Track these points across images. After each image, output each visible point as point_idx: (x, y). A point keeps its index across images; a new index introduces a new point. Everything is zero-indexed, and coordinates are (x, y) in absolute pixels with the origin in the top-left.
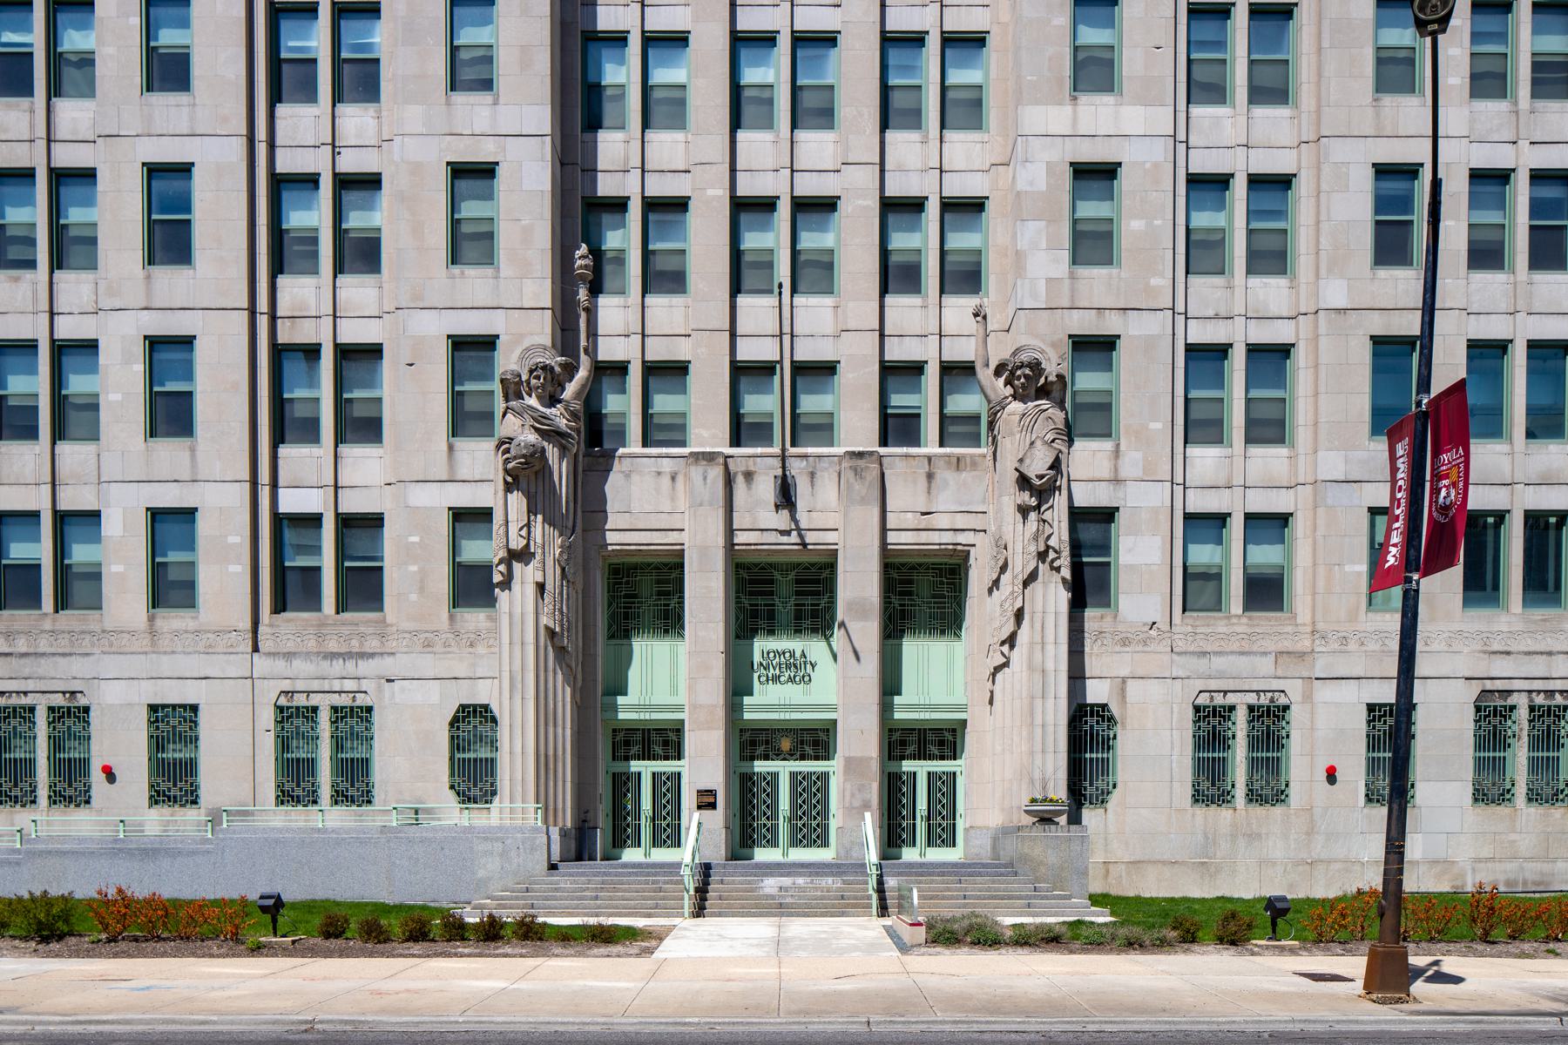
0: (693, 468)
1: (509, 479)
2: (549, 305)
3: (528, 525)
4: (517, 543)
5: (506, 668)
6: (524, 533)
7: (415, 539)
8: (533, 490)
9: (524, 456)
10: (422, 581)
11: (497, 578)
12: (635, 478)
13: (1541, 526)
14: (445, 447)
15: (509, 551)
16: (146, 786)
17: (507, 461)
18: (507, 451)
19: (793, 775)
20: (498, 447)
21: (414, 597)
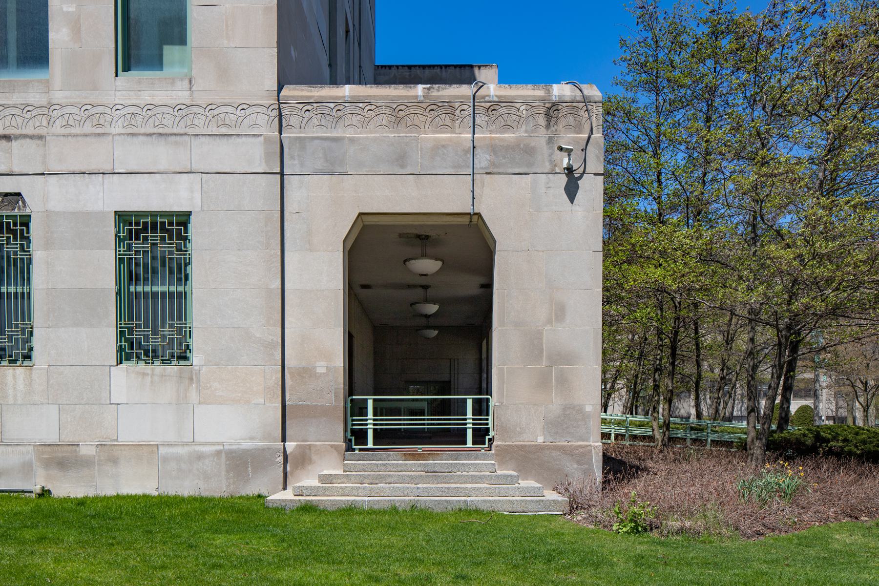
16: (111, 333)
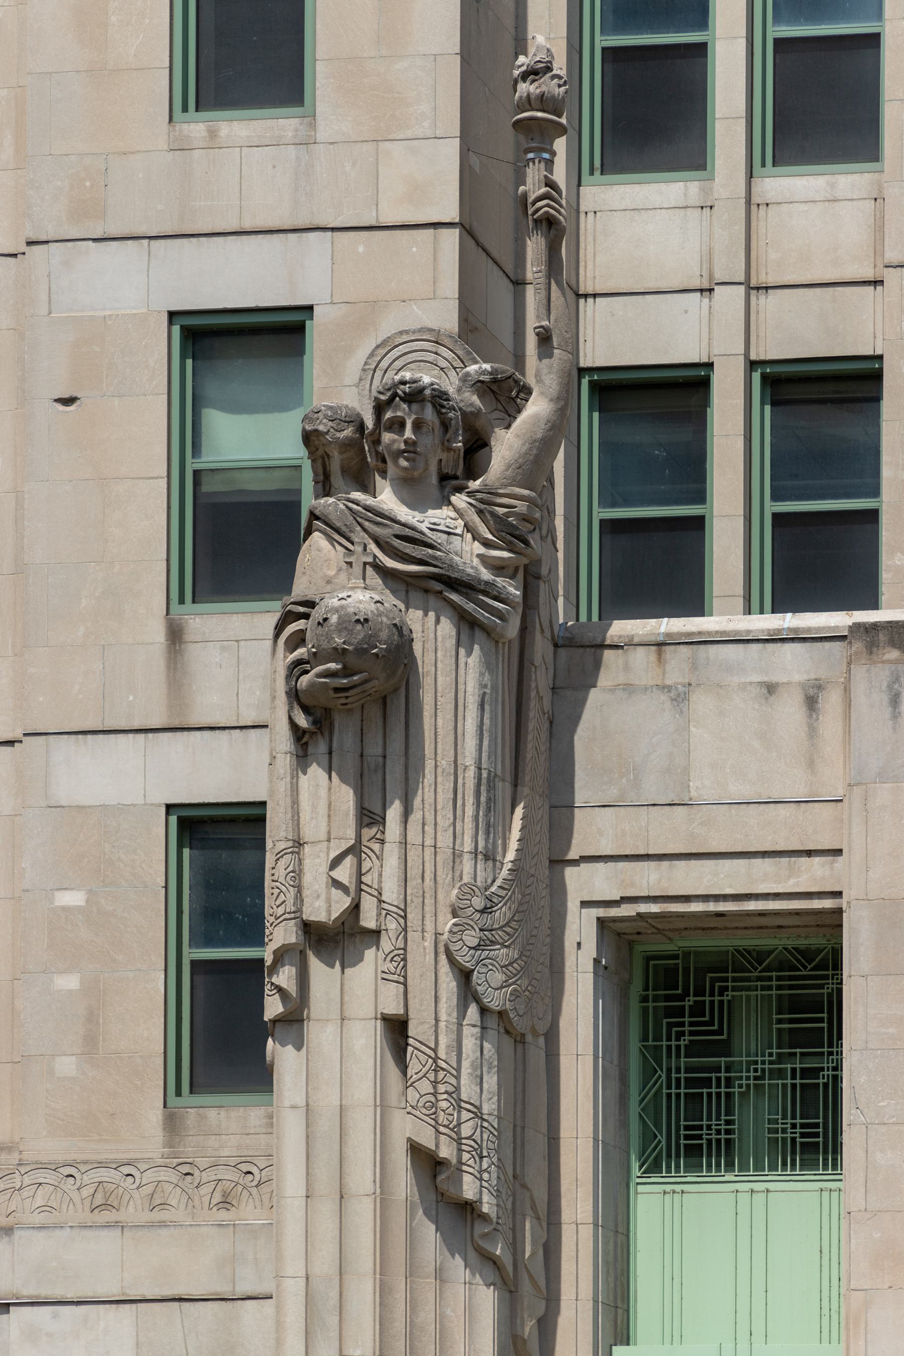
0: (859, 672)
1: (302, 721)
2: (452, 213)
3: (355, 850)
4: (324, 907)
5: (294, 1266)
6: (344, 873)
7: (73, 898)
8: (374, 749)
9: (338, 654)
10: (91, 1017)
11: (273, 1007)
12: (702, 703)
13: (818, 398)
14: (158, 634)
15: (307, 928)
17: (297, 668)
18: (298, 639)
20: (279, 629)
21: (67, 1066)
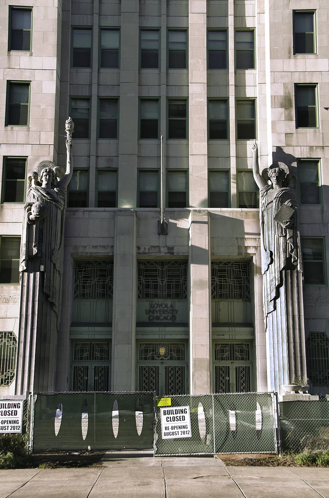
19: (166, 368)
